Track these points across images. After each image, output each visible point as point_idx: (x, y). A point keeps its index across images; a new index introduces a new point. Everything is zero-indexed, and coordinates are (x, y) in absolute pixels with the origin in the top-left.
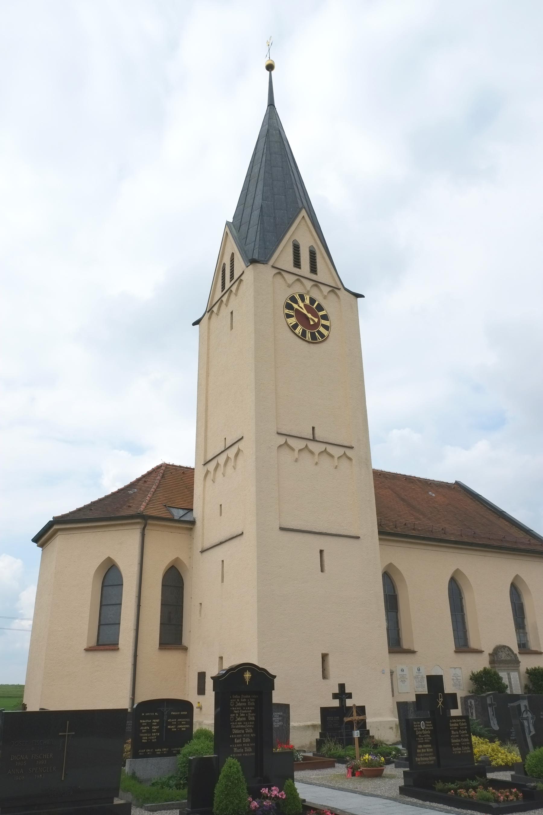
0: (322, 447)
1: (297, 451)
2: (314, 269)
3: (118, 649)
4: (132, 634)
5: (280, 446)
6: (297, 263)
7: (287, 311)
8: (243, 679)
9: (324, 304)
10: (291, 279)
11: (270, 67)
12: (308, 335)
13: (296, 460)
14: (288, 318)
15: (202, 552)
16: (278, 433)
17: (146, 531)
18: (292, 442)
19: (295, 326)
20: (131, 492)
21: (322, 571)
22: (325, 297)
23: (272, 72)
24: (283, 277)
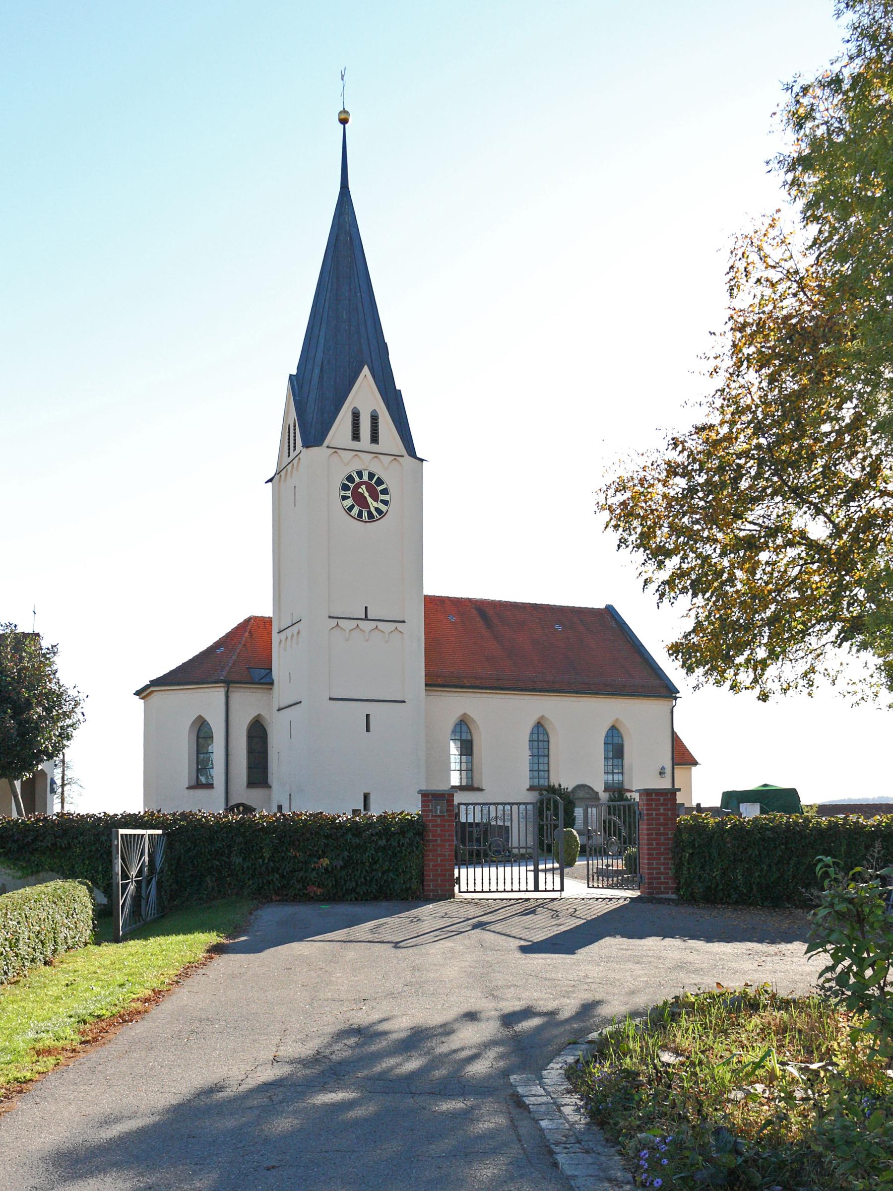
0: (374, 624)
1: (348, 631)
2: (375, 439)
6: (356, 436)
7: (343, 493)
11: (344, 121)
12: (365, 515)
16: (330, 617)
17: (230, 689)
19: (351, 508)
20: (218, 651)
21: (368, 730)
23: (347, 126)
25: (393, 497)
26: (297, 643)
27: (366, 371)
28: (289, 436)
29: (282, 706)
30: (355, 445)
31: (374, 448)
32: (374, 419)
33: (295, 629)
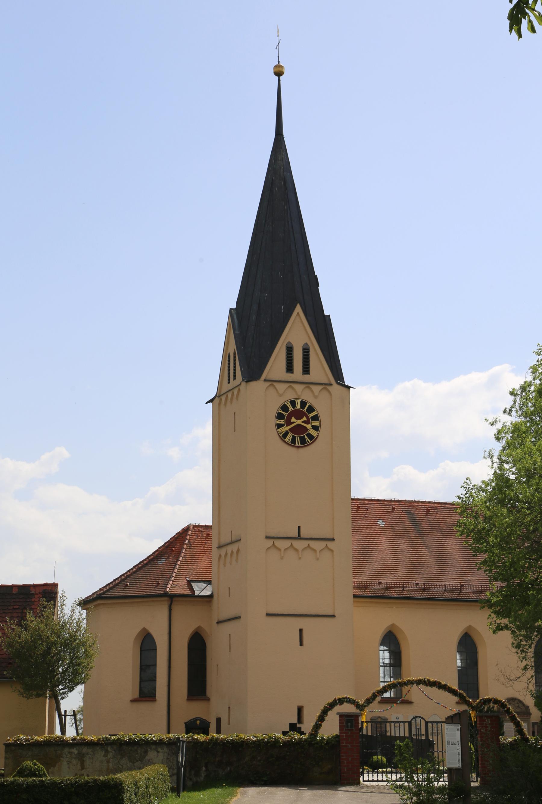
0: (305, 543)
1: (283, 550)
2: (306, 370)
3: (156, 700)
4: (166, 689)
5: (269, 548)
6: (290, 368)
7: (279, 422)
8: (197, 724)
9: (315, 405)
10: (282, 387)
11: (279, 73)
12: (298, 440)
13: (282, 558)
14: (278, 428)
15: (218, 623)
17: (173, 607)
18: (278, 543)
21: (301, 644)
22: (316, 397)
24: (275, 388)
25: (324, 422)
26: (237, 560)
27: (298, 309)
28: (229, 364)
29: (221, 619)
30: (289, 377)
31: (306, 378)
32: (306, 352)
33: (235, 547)
